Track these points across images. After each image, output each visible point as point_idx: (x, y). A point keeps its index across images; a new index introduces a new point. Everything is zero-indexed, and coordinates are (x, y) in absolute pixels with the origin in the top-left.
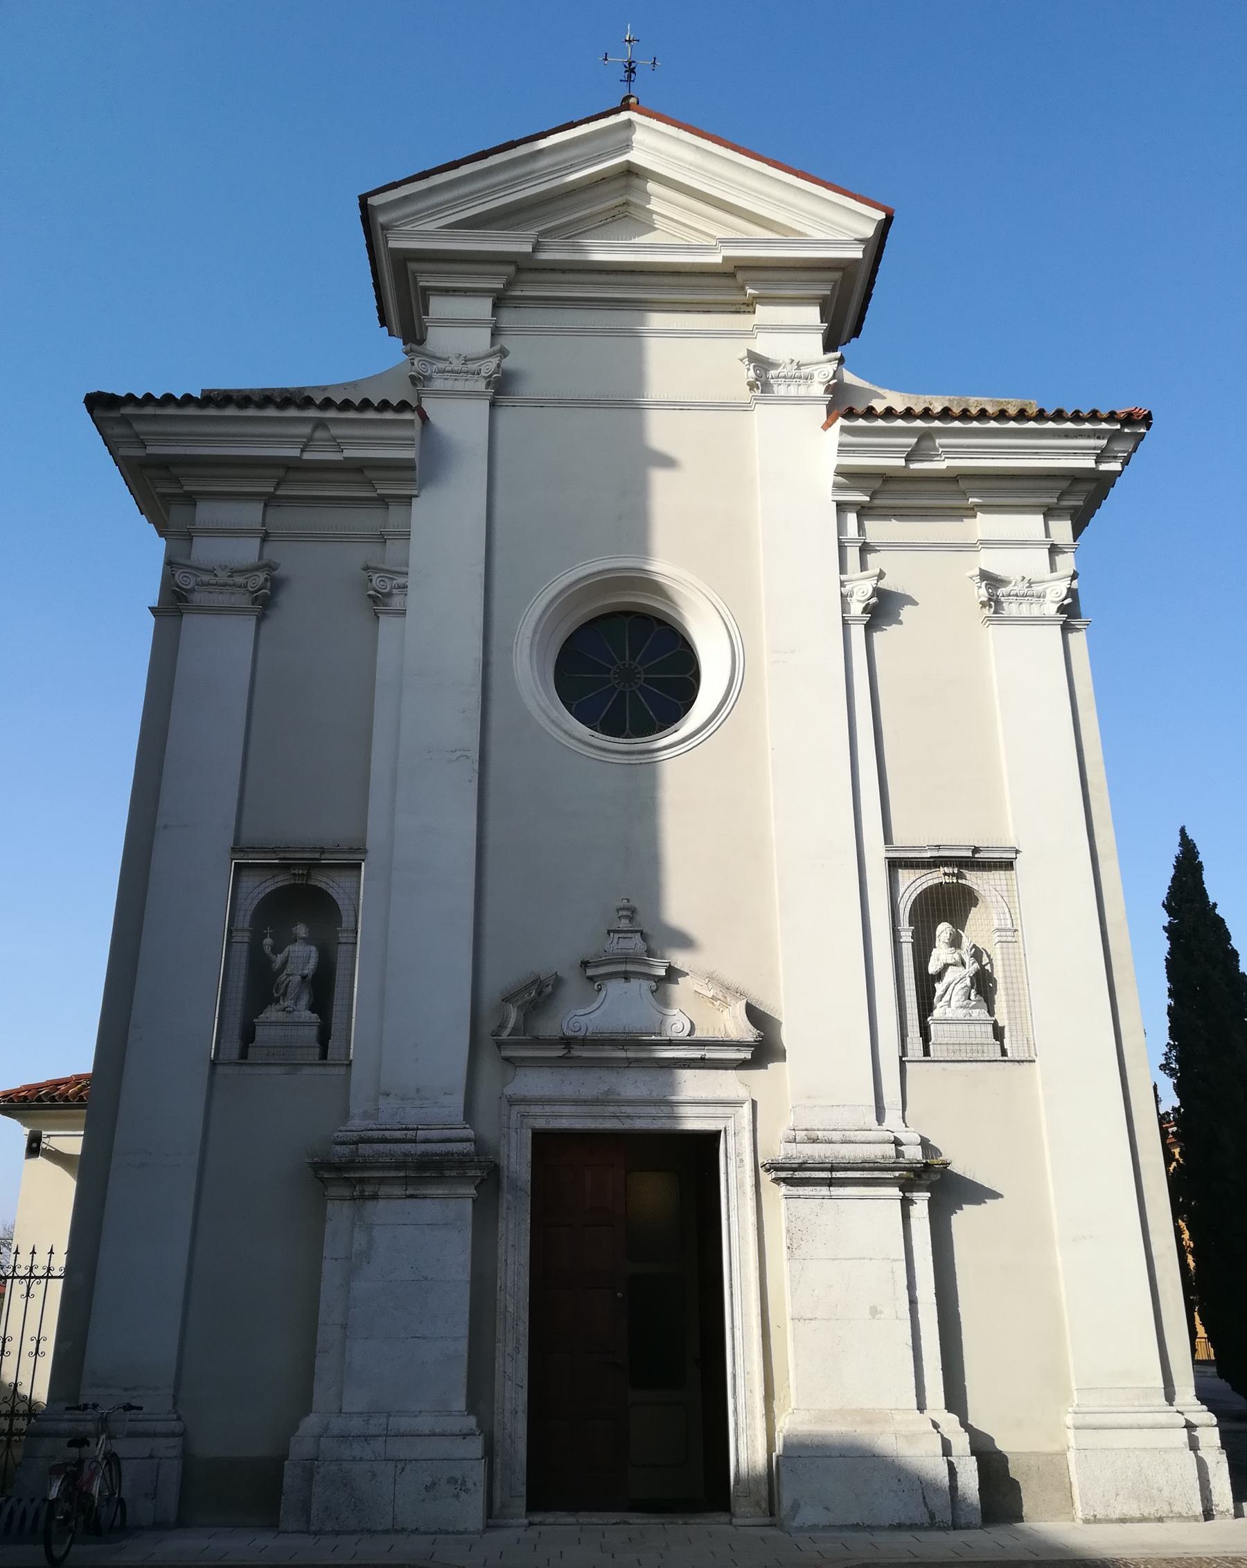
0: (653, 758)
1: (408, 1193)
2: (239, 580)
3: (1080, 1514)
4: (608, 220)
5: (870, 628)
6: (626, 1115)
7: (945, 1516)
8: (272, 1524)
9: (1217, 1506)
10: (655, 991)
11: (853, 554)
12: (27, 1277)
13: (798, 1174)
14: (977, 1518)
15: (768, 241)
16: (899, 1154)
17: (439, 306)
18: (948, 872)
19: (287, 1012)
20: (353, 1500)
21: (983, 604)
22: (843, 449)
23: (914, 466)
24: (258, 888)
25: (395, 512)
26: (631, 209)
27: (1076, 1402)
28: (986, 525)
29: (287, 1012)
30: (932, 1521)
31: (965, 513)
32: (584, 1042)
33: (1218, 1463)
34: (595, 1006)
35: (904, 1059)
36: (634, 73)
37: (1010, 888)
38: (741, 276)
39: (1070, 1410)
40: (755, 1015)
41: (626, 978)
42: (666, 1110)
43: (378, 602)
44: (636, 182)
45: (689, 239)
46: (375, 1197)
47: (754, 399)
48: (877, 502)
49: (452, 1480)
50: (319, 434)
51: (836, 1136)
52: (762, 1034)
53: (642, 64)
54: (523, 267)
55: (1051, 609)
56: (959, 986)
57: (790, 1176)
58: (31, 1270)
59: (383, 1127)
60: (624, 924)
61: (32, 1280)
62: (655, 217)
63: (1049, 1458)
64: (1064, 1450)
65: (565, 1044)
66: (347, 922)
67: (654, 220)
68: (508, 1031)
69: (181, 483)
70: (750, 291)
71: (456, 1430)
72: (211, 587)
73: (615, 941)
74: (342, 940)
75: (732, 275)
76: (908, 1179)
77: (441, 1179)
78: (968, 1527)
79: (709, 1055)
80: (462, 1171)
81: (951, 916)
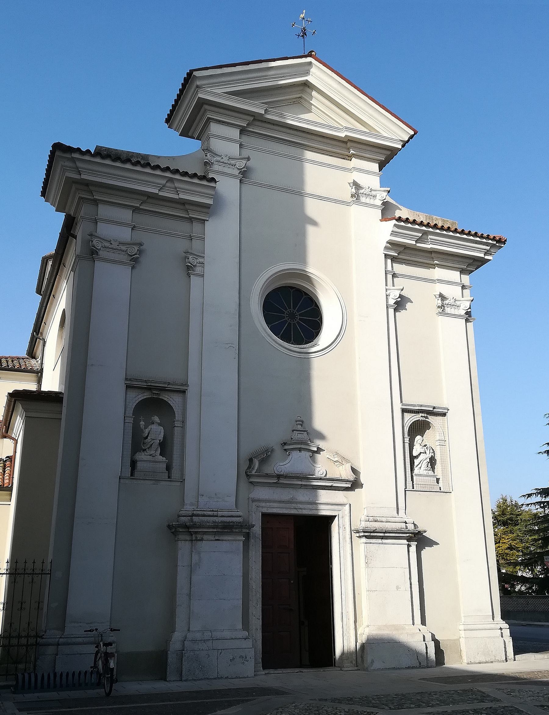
0: (309, 356)
1: (216, 538)
2: (124, 248)
3: (465, 661)
4: (291, 103)
5: (396, 310)
6: (300, 508)
7: (425, 664)
8: (164, 678)
9: (508, 657)
10: (311, 457)
11: (390, 277)
12: (32, 574)
13: (372, 534)
14: (434, 664)
15: (365, 132)
16: (407, 527)
17: (214, 128)
18: (423, 416)
19: (153, 456)
20: (200, 666)
21: (439, 307)
22: (393, 233)
23: (418, 245)
24: (137, 397)
25: (196, 226)
26: (302, 101)
27: (463, 621)
28: (439, 273)
29: (153, 456)
30: (420, 665)
31: (431, 266)
32: (286, 477)
33: (509, 641)
34: (287, 461)
35: (406, 489)
36: (306, 35)
37: (444, 424)
38: (349, 144)
39: (461, 624)
40: (354, 470)
41: (300, 451)
42: (313, 507)
43: (189, 269)
44: (308, 90)
45: (329, 123)
46: (202, 540)
47: (353, 202)
48: (400, 257)
49: (241, 657)
50: (168, 184)
51: (384, 519)
52: (357, 477)
53: (309, 31)
54: (257, 119)
55: (463, 312)
56: (425, 461)
57: (369, 535)
58: (33, 570)
59: (203, 510)
60: (299, 427)
61: (34, 575)
62: (312, 107)
63: (454, 641)
64: (458, 638)
65: (278, 477)
66: (178, 416)
67: (312, 108)
68: (255, 471)
69: (93, 194)
70: (352, 151)
71: (240, 636)
72: (109, 249)
73: (297, 435)
74: (176, 425)
75: (346, 143)
76: (411, 537)
77: (231, 533)
78: (431, 667)
79: (334, 485)
80: (240, 530)
81: (420, 433)
